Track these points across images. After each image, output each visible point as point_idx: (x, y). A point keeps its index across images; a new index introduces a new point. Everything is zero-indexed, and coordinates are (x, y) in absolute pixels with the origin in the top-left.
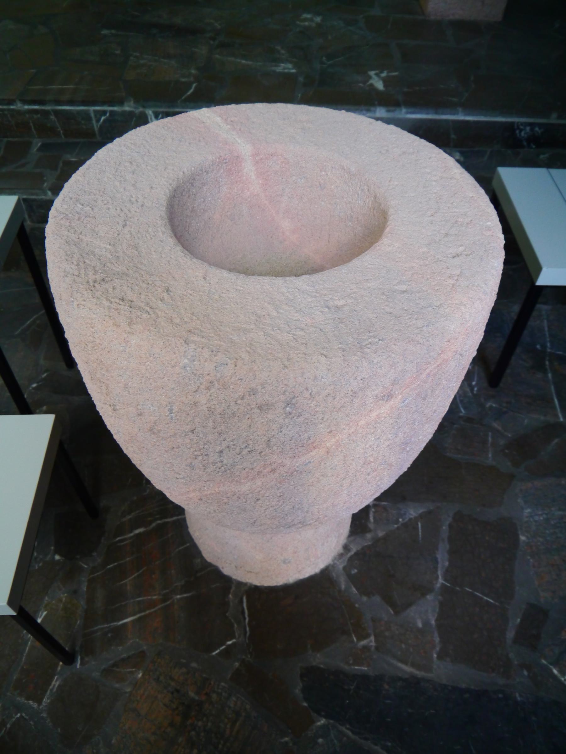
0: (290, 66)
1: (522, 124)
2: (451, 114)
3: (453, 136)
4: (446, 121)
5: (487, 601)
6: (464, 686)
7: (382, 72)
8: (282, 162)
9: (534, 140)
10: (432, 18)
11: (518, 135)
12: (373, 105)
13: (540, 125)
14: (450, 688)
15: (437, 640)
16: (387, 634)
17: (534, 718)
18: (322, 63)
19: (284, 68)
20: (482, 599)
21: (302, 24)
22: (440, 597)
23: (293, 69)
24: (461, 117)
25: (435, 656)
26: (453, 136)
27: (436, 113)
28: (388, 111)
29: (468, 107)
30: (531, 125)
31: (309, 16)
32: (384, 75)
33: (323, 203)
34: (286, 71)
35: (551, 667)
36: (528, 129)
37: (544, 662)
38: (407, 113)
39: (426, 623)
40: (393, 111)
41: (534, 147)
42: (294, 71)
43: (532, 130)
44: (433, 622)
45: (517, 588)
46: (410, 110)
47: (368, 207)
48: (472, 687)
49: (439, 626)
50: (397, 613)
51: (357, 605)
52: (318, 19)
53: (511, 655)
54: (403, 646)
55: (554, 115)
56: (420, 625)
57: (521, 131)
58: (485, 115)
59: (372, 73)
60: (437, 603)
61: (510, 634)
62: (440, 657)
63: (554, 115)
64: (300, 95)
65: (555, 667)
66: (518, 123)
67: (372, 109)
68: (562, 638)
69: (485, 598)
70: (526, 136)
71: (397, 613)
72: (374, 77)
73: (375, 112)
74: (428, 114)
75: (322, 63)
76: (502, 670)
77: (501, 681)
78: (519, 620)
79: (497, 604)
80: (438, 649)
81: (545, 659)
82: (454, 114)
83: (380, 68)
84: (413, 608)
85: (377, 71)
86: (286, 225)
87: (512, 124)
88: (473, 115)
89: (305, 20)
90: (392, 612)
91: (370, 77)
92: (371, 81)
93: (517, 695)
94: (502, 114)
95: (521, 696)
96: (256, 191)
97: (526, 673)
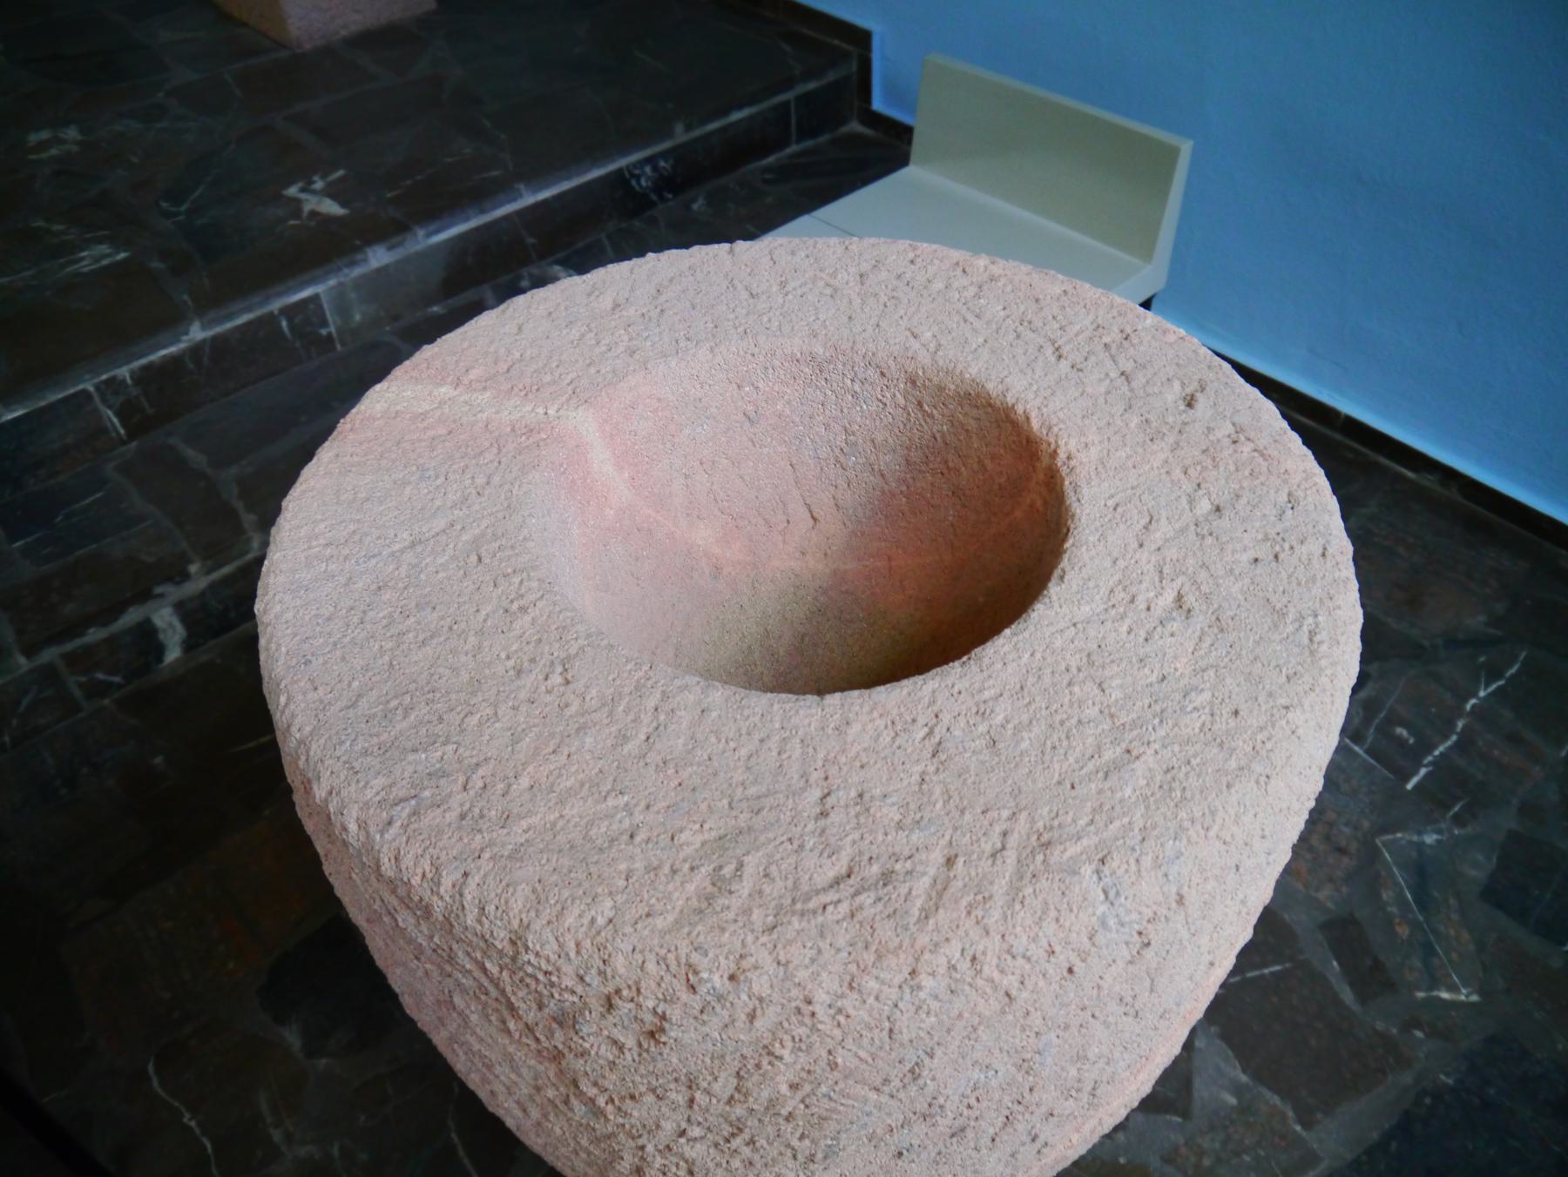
0: (104, 249)
1: (635, 165)
2: (509, 201)
3: (530, 240)
4: (506, 218)
5: (1272, 974)
6: (1375, 1136)
7: (311, 182)
8: (655, 411)
9: (670, 184)
10: (308, 46)
11: (637, 187)
12: (359, 249)
13: (664, 155)
14: (1364, 1158)
15: (1276, 1100)
16: (1207, 1162)
17: (1492, 1091)
18: (167, 215)
19: (98, 259)
20: (1262, 977)
21: (44, 155)
22: (1213, 1029)
23: (118, 251)
24: (529, 199)
25: (1298, 1128)
26: (530, 240)
27: (483, 211)
28: (391, 248)
29: (535, 174)
30: (649, 160)
31: (45, 135)
32: (319, 185)
33: (766, 450)
34: (105, 262)
35: (1435, 993)
36: (648, 169)
37: (1421, 995)
38: (429, 235)
39: (1238, 1090)
40: (400, 244)
41: (670, 196)
42: (122, 255)
43: (655, 169)
44: (1244, 1078)
45: (1286, 916)
46: (432, 227)
47: (897, 406)
48: (1387, 1126)
49: (1257, 1076)
50: (1186, 1114)
51: (1122, 1160)
52: (72, 133)
53: (1380, 1026)
54: (1247, 1158)
55: (679, 128)
56: (1232, 1101)
57: (638, 178)
58: (568, 178)
59: (292, 191)
60: (1218, 1042)
61: (1347, 995)
62: (1307, 1125)
63: (679, 128)
64: (185, 297)
65: (1439, 990)
66: (627, 167)
67: (359, 257)
68: (1404, 938)
69: (1266, 971)
70: (650, 184)
71: (1186, 1114)
72: (303, 196)
73: (365, 260)
74: (467, 219)
75: (167, 215)
76: (1391, 1060)
77: (1407, 1078)
78: (1335, 963)
79: (1288, 965)
80: (1290, 1114)
81: (1419, 989)
82: (514, 200)
83: (303, 174)
84: (1197, 1083)
85: (300, 184)
86: (704, 535)
87: (619, 172)
88: (547, 186)
89: (42, 146)
90: (1179, 1120)
91: (297, 202)
92: (307, 208)
93: (1443, 1077)
94: (596, 162)
95: (1447, 1075)
96: (623, 499)
97: (1419, 1034)
